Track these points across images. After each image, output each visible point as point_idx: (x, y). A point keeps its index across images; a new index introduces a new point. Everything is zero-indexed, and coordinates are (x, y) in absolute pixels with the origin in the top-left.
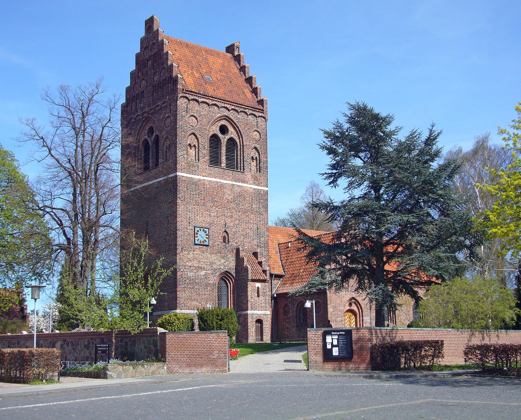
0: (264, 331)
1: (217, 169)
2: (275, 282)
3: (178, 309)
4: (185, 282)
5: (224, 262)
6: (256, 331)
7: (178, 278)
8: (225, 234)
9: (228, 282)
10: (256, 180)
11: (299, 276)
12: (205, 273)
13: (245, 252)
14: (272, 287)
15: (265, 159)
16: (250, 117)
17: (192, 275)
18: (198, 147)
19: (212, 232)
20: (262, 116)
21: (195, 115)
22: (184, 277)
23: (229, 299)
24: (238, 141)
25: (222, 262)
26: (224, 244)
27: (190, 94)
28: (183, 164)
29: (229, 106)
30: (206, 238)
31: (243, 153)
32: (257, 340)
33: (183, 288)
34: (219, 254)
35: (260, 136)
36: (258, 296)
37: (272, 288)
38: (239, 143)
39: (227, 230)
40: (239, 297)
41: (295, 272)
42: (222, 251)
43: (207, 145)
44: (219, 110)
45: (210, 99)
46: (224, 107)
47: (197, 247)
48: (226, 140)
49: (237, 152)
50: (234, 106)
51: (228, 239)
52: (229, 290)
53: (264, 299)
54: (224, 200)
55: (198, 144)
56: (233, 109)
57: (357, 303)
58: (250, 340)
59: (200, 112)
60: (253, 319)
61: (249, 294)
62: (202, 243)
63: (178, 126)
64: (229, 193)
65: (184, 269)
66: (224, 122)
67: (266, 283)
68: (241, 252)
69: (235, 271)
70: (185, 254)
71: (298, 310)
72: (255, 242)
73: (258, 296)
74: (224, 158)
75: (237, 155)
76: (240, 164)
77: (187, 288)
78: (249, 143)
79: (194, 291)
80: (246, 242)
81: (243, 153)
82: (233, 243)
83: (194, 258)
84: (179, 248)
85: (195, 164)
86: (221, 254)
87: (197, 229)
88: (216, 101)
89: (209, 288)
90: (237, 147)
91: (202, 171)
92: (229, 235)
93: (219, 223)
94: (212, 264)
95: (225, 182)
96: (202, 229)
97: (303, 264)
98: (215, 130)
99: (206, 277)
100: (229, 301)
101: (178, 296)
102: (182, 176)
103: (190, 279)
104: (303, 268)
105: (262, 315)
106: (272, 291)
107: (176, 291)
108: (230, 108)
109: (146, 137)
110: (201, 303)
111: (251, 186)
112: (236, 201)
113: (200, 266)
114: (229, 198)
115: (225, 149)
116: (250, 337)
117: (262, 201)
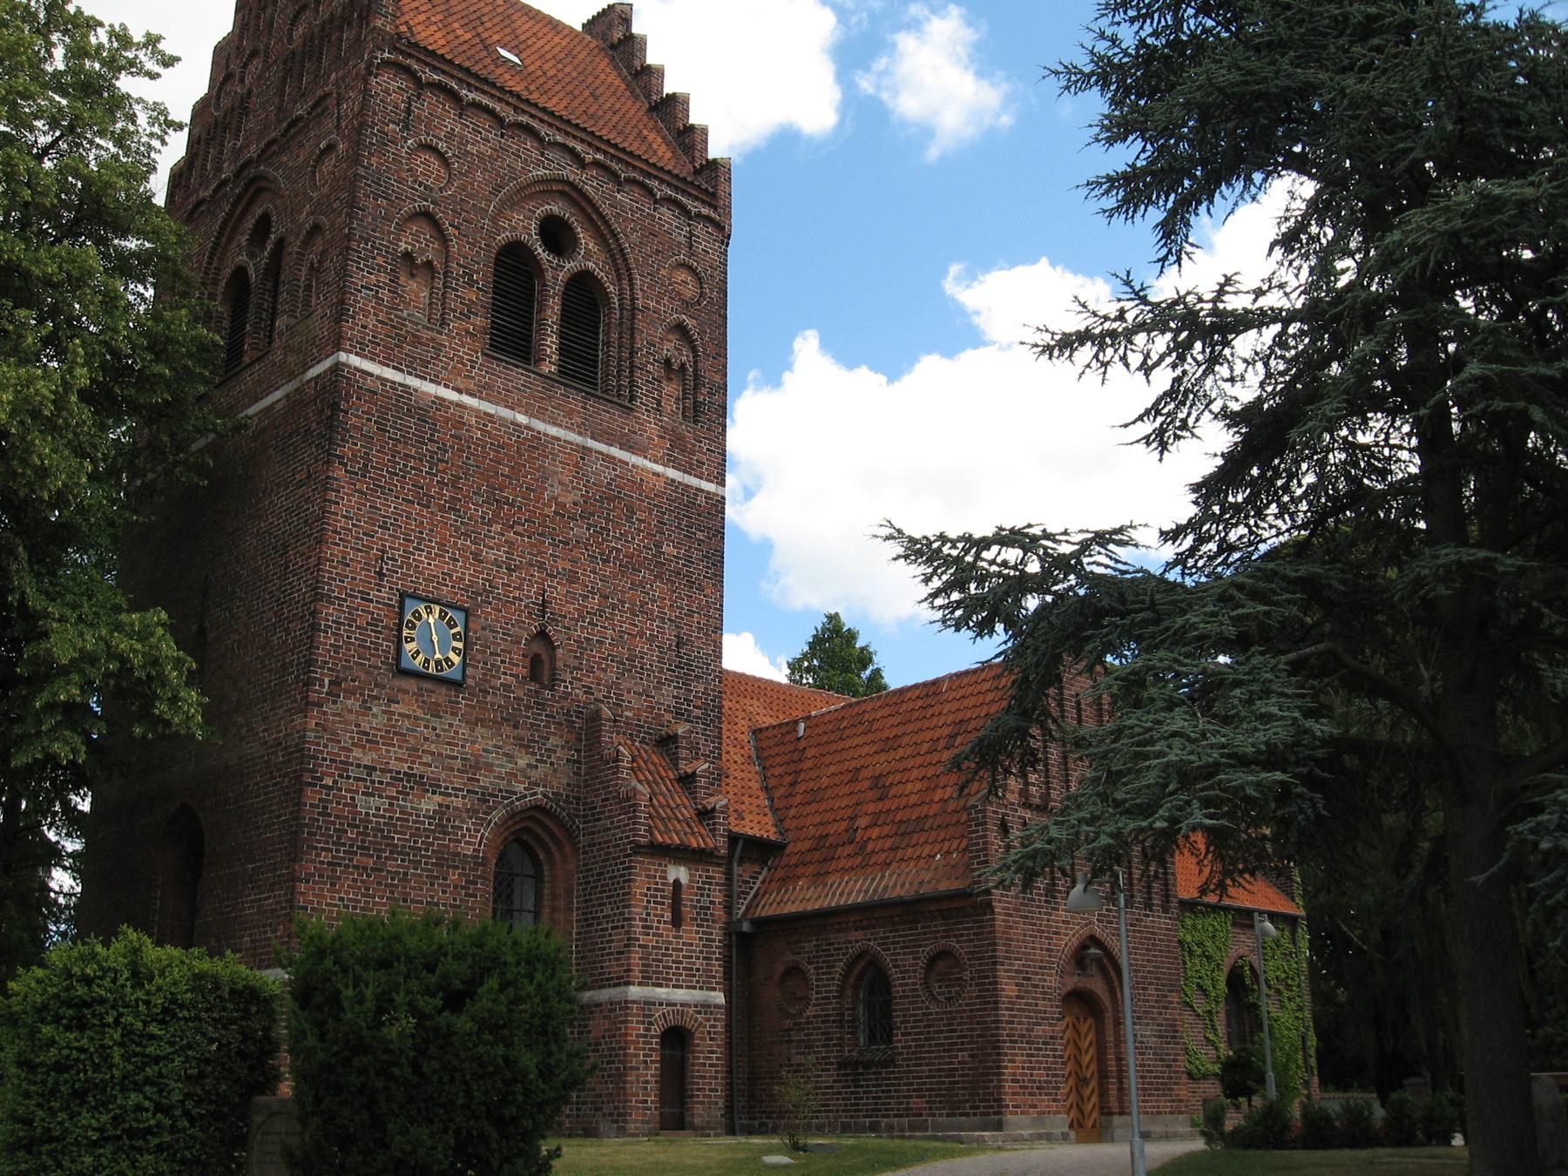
1: (517, 376)
4: (339, 838)
8: (537, 648)
10: (679, 452)
12: (440, 805)
13: (624, 734)
15: (717, 378)
17: (378, 809)
18: (445, 274)
19: (484, 628)
20: (708, 219)
21: (442, 146)
22: (336, 816)
25: (522, 763)
27: (426, 64)
33: (329, 864)
34: (506, 730)
38: (616, 300)
40: (592, 925)
43: (483, 273)
46: (564, 147)
47: (411, 685)
50: (605, 153)
53: (701, 939)
54: (545, 505)
56: (596, 164)
57: (1108, 965)
58: (635, 1121)
59: (463, 142)
62: (432, 670)
64: (566, 480)
66: (556, 208)
70: (350, 711)
71: (849, 992)
72: (667, 696)
73: (677, 922)
74: (551, 343)
77: (347, 866)
80: (629, 692)
82: (572, 687)
83: (392, 734)
85: (426, 334)
86: (516, 727)
88: (532, 116)
89: (454, 876)
91: (454, 367)
94: (473, 766)
95: (553, 431)
98: (523, 226)
99: (443, 826)
105: (691, 1010)
108: (589, 158)
109: (243, 258)
111: (659, 468)
113: (417, 769)
114: (567, 500)
117: (700, 535)
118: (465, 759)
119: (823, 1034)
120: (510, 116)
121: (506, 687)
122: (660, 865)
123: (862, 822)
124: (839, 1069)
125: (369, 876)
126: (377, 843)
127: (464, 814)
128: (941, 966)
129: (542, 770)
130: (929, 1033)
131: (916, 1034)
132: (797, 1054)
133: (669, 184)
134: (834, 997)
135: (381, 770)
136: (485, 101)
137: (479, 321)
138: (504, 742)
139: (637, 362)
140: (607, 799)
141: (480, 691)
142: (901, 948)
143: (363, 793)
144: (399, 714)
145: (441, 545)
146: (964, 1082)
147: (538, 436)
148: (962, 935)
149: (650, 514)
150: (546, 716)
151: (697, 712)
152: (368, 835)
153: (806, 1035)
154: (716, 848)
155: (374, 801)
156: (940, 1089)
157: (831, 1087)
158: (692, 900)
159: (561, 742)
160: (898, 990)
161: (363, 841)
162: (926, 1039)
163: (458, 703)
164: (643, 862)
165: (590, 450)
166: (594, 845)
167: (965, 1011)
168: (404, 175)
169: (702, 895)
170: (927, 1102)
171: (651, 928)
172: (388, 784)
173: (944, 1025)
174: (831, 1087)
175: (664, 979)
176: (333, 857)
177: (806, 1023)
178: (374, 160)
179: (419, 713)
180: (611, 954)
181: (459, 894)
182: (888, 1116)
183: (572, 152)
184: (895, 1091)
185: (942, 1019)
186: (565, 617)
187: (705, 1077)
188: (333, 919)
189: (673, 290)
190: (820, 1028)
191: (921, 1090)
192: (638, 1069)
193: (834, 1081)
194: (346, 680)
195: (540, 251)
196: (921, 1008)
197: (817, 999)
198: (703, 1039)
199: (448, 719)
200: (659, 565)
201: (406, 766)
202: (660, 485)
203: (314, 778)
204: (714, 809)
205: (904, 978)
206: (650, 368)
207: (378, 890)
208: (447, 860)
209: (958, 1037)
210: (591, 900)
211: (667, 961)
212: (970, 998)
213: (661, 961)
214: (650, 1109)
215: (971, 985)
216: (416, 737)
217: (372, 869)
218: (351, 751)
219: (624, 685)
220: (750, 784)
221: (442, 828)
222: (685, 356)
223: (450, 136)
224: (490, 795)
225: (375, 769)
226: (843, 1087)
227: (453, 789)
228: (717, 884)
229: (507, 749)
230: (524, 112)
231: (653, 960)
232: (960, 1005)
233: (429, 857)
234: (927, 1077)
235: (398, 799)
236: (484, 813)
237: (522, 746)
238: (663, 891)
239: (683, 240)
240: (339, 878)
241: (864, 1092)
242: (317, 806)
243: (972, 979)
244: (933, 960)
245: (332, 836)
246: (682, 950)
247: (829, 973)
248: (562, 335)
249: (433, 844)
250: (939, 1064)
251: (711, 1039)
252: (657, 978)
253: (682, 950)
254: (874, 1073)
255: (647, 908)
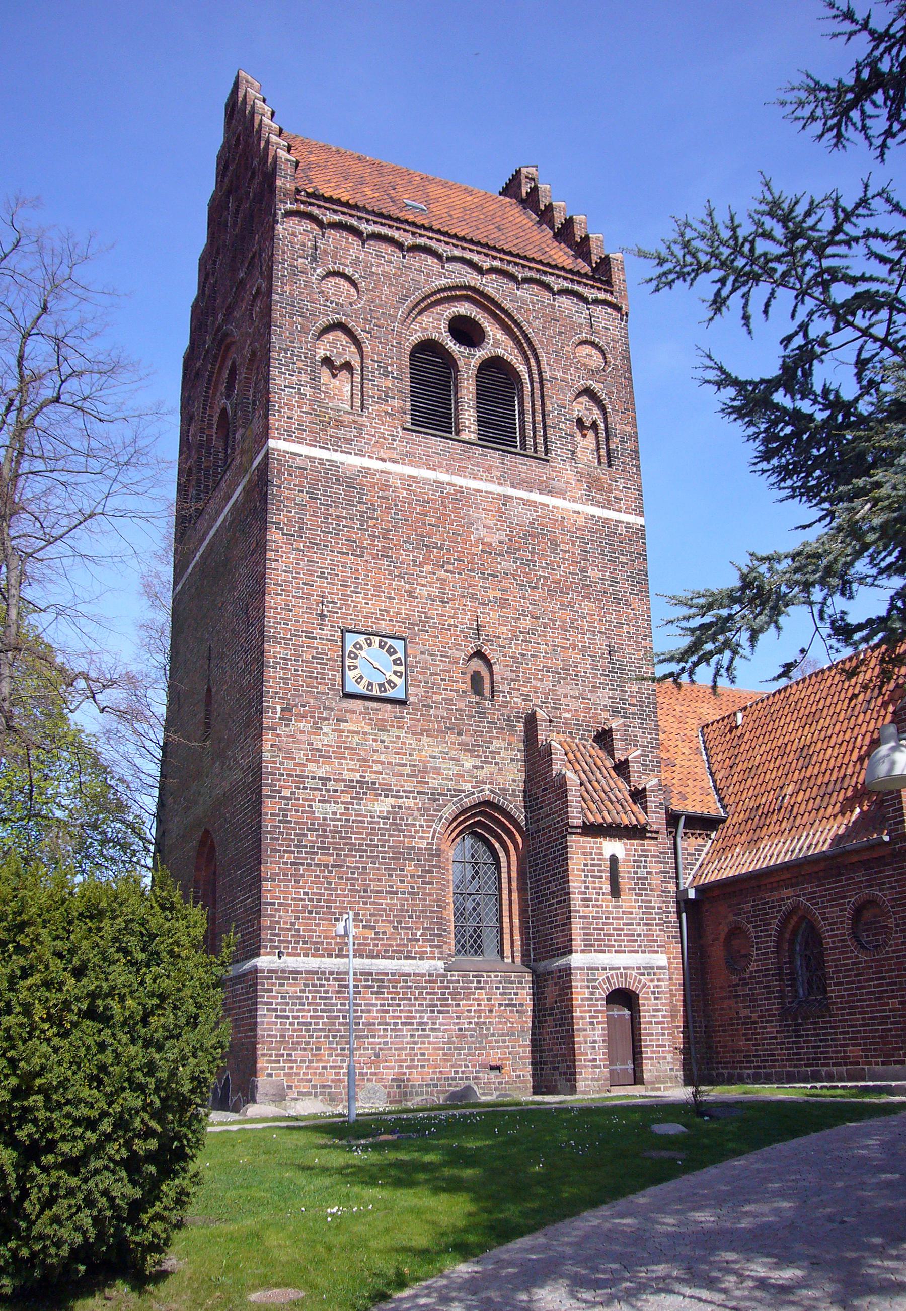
0: (646, 1040)
1: (436, 443)
2: (688, 844)
3: (268, 954)
4: (300, 841)
5: (475, 767)
6: (610, 1040)
7: (268, 823)
8: (477, 664)
9: (497, 845)
11: (779, 810)
12: (393, 807)
13: (564, 733)
14: (676, 863)
16: (563, 299)
18: (362, 370)
19: (422, 653)
20: (604, 302)
21: (349, 271)
22: (296, 823)
23: (506, 913)
24: (522, 368)
26: (475, 699)
28: (296, 413)
29: (482, 257)
30: (395, 672)
31: (543, 405)
32: (615, 1081)
34: (451, 737)
35: (605, 358)
36: (616, 892)
37: (677, 868)
38: (527, 376)
39: (486, 650)
41: (764, 800)
42: (464, 725)
44: (443, 267)
45: (405, 231)
46: (462, 260)
48: (475, 362)
49: (521, 404)
50: (502, 260)
51: (492, 682)
52: (504, 876)
55: (362, 362)
56: (493, 270)
58: (586, 1079)
60: (594, 987)
61: (576, 885)
62: (375, 692)
63: (275, 297)
64: (491, 523)
65: (297, 788)
66: (464, 309)
67: (646, 842)
68: (542, 727)
69: (525, 802)
70: (303, 732)
71: (786, 946)
72: (603, 697)
73: (616, 892)
74: (468, 417)
75: (522, 413)
76: (534, 437)
77: (309, 865)
78: (564, 373)
79: (341, 878)
81: (543, 405)
84: (273, 710)
85: (347, 418)
86: (460, 734)
87: (351, 639)
89: (410, 868)
90: (522, 391)
92: (496, 668)
93: (451, 621)
94: (421, 772)
96: (377, 639)
97: (794, 765)
99: (396, 824)
100: (506, 920)
101: (267, 897)
102: (292, 453)
103: (325, 831)
104: (795, 779)
105: (634, 973)
106: (677, 878)
107: (258, 880)
108: (486, 266)
110: (374, 927)
111: (578, 507)
112: (519, 550)
114: (494, 539)
115: (472, 388)
116: (582, 1067)
117: (623, 559)
118: (414, 765)
119: (764, 987)
120: (408, 240)
121: (448, 701)
122: (596, 843)
123: (789, 790)
124: (781, 1021)
125: (330, 872)
126: (335, 843)
127: (416, 813)
128: (867, 915)
129: (487, 769)
130: (859, 981)
131: (847, 983)
132: (744, 1007)
133: (565, 278)
134: (772, 952)
135: (335, 780)
136: (384, 231)
137: (396, 403)
138: (450, 748)
139: (549, 422)
140: (546, 789)
141: (424, 706)
142: (828, 901)
143: (320, 801)
144: (349, 732)
145: (377, 587)
146: (896, 1029)
147: (460, 490)
148: (884, 883)
149: (574, 545)
150: (488, 723)
151: (634, 709)
152: (327, 837)
153: (750, 989)
154: (647, 824)
155: (330, 808)
156: (874, 1038)
157: (775, 1038)
158: (629, 872)
159: (504, 744)
160: (828, 942)
161: (323, 842)
162: (857, 988)
163: (403, 718)
164: (579, 841)
165: (511, 497)
166: (539, 831)
167: (892, 958)
168: (316, 296)
169: (639, 867)
170: (863, 1051)
171: (591, 900)
172: (342, 792)
173: (874, 973)
174: (775, 1038)
175: (605, 945)
176: (295, 858)
177: (750, 978)
178: (287, 288)
179: (368, 729)
180: (557, 926)
181: (416, 883)
182: (827, 1065)
183: (470, 263)
184: (833, 1040)
185: (871, 967)
186: (499, 637)
187: (652, 1034)
188: (299, 911)
189: (578, 362)
190: (762, 982)
191: (856, 1038)
192: (585, 1030)
193: (778, 1032)
194: (296, 706)
195: (452, 345)
196: (850, 958)
197: (757, 955)
198: (646, 999)
199: (395, 732)
200: (586, 589)
201: (358, 775)
202: (581, 521)
203: (272, 791)
204: (644, 789)
205: (832, 930)
206: (562, 426)
207: (340, 884)
208: (403, 853)
209: (889, 984)
210: (539, 880)
211: (608, 929)
212: (897, 945)
213: (602, 929)
214: (599, 1067)
215: (896, 932)
216: (365, 750)
217: (333, 866)
218: (305, 765)
219: (560, 691)
220: (696, 770)
221: (396, 826)
222: (596, 414)
223: (356, 262)
224: (439, 794)
225: (329, 780)
226: (786, 1037)
227: (404, 791)
228: (653, 856)
229: (453, 753)
230: (421, 236)
231: (594, 929)
232: (888, 953)
233: (386, 852)
234: (861, 1025)
235: (352, 804)
236: (435, 811)
237: (466, 750)
238: (600, 866)
239: (583, 321)
240: (303, 876)
241: (805, 1042)
242: (278, 815)
243: (897, 925)
244: (858, 911)
245: (293, 840)
246: (622, 918)
247: (766, 930)
248: (479, 410)
249: (388, 841)
250: (872, 1012)
251: (656, 998)
252: (599, 946)
253: (622, 918)
254: (812, 1023)
255: (585, 882)
